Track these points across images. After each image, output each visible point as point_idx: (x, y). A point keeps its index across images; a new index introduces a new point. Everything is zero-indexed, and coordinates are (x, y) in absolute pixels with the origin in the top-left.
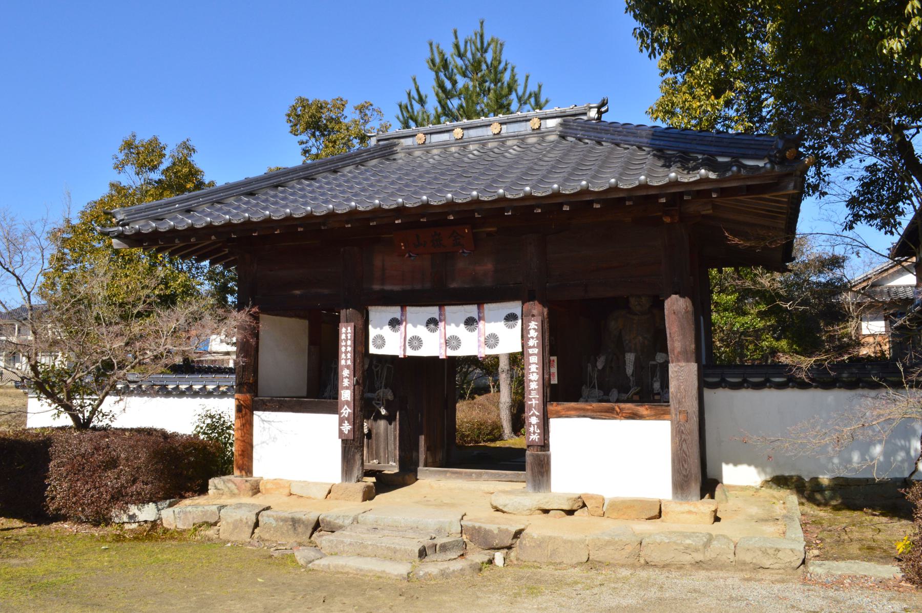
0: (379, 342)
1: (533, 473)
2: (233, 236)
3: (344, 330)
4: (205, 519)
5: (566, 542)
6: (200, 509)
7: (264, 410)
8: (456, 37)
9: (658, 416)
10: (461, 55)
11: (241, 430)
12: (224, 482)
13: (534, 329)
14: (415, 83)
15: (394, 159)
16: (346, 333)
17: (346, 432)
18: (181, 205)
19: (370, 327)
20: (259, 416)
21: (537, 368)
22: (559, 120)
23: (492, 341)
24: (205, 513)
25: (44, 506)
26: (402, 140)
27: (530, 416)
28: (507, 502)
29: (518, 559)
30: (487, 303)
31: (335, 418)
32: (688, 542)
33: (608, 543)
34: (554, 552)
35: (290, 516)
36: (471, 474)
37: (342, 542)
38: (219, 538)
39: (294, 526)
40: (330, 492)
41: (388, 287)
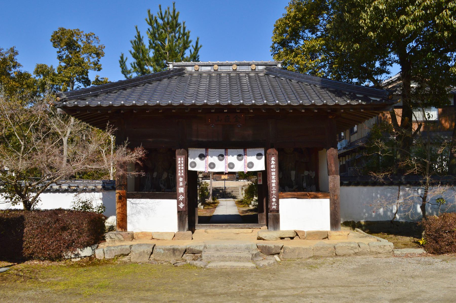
0: (193, 165)
1: (273, 223)
2: (134, 112)
3: (179, 159)
4: (122, 253)
5: (304, 249)
6: (119, 248)
7: (133, 198)
8: (160, 9)
9: (325, 197)
10: (162, 18)
11: (121, 208)
12: (115, 235)
13: (274, 160)
14: (137, 30)
15: (184, 77)
16: (181, 161)
17: (182, 208)
18: (93, 93)
19: (189, 158)
20: (130, 201)
21: (275, 177)
22: (264, 67)
23: (212, 166)
24: (122, 250)
25: (23, 253)
26: (186, 67)
27: (272, 198)
28: (266, 235)
29: (283, 258)
30: (248, 148)
31: (175, 201)
32: (352, 245)
33: (322, 248)
34: (299, 253)
35: (172, 247)
36: (222, 226)
37: (213, 256)
38: (130, 261)
39: (174, 252)
40: (174, 236)
41: (200, 139)
